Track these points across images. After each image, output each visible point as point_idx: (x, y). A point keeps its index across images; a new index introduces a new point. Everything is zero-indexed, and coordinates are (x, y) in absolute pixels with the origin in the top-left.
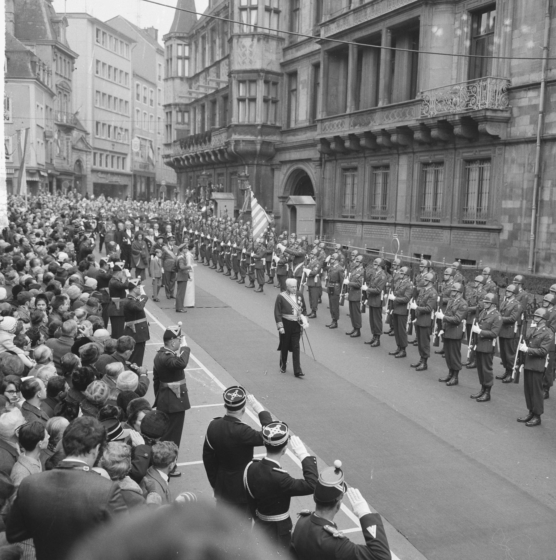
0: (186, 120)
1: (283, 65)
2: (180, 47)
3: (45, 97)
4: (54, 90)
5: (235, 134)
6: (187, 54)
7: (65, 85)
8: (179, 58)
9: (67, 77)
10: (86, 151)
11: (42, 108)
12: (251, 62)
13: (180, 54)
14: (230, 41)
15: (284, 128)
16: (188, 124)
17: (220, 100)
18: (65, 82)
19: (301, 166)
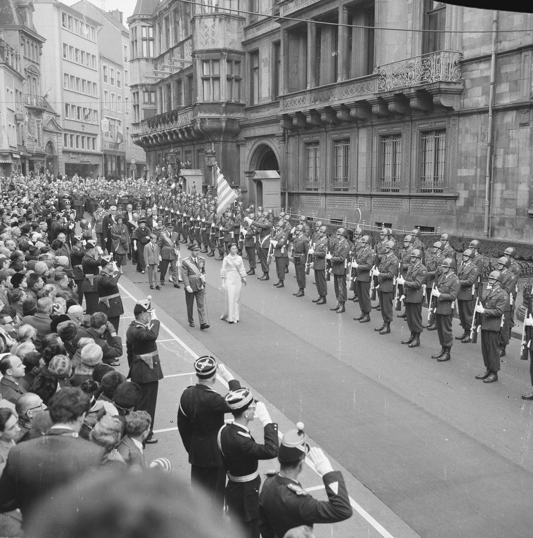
0: (153, 100)
2: (144, 29)
3: (14, 82)
4: (23, 74)
5: (201, 113)
7: (34, 69)
8: (144, 39)
9: (36, 61)
10: (57, 133)
11: (12, 92)
12: (213, 42)
15: (248, 105)
16: (155, 103)
18: (33, 66)
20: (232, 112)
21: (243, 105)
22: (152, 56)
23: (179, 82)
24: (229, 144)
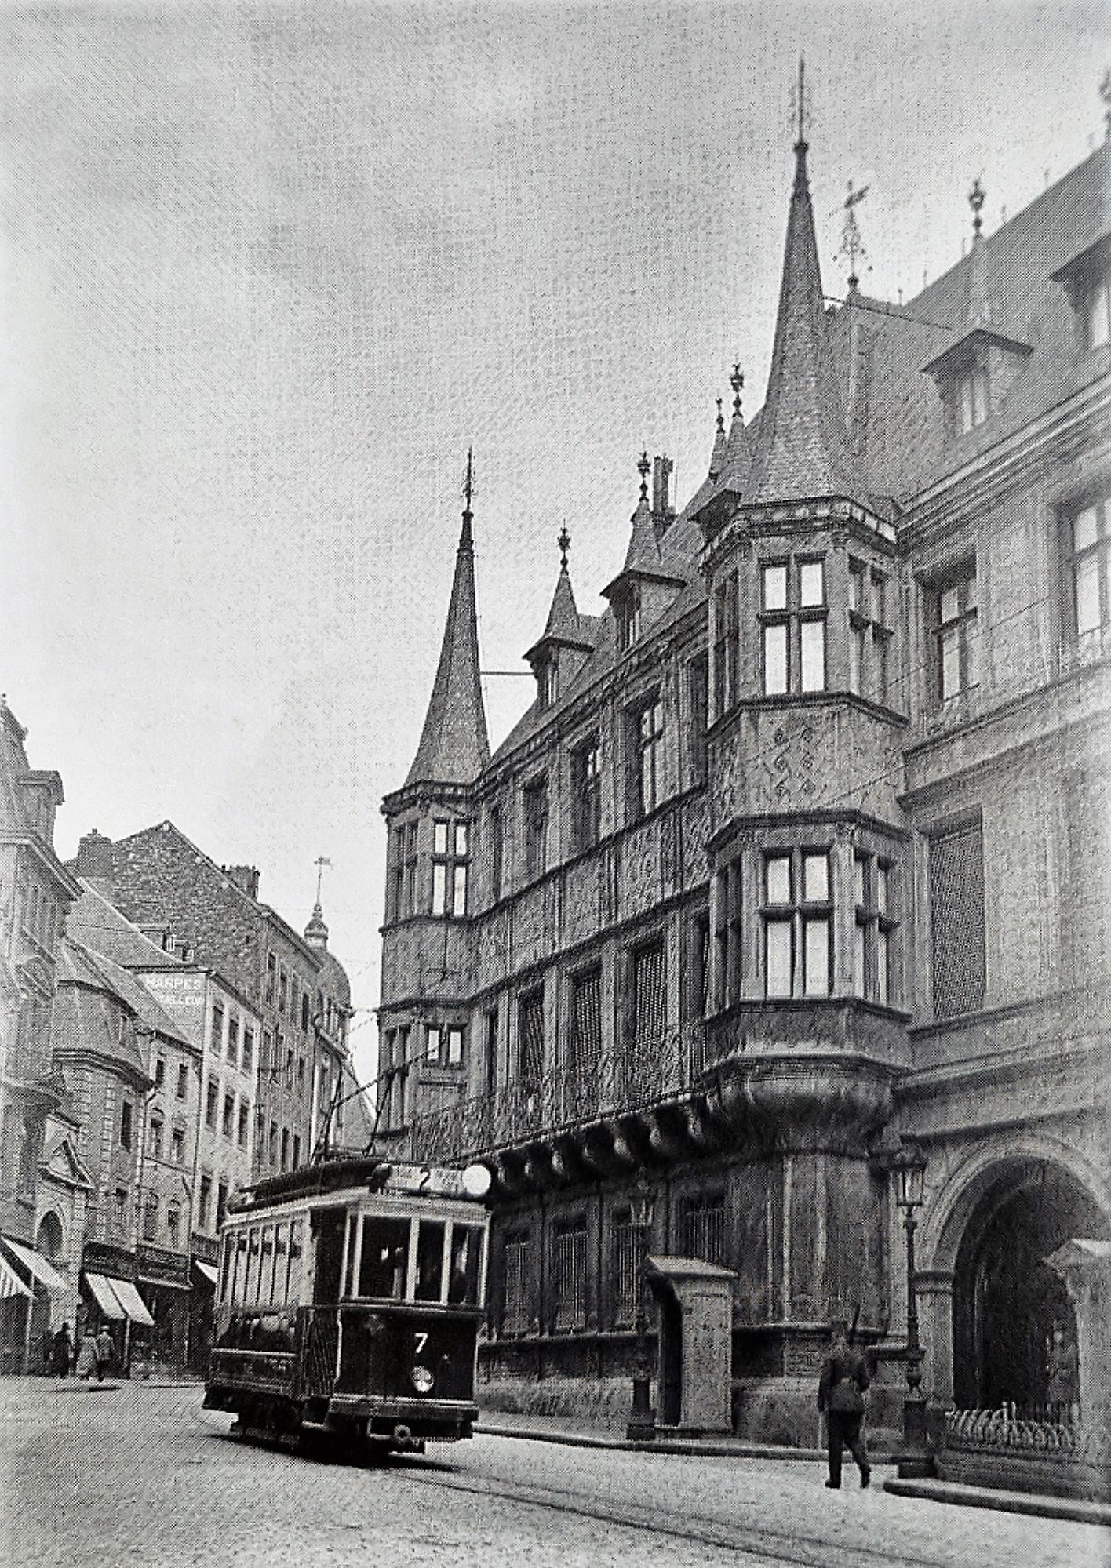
0: (455, 1056)
1: (906, 804)
2: (441, 829)
5: (757, 1039)
6: (461, 850)
8: (438, 860)
10: (70, 1187)
12: (808, 789)
13: (440, 848)
14: (729, 721)
15: (926, 1019)
16: (461, 1067)
17: (612, 960)
19: (1033, 1147)
20: (871, 1038)
21: (903, 1019)
22: (459, 911)
23: (585, 979)
24: (847, 1168)
